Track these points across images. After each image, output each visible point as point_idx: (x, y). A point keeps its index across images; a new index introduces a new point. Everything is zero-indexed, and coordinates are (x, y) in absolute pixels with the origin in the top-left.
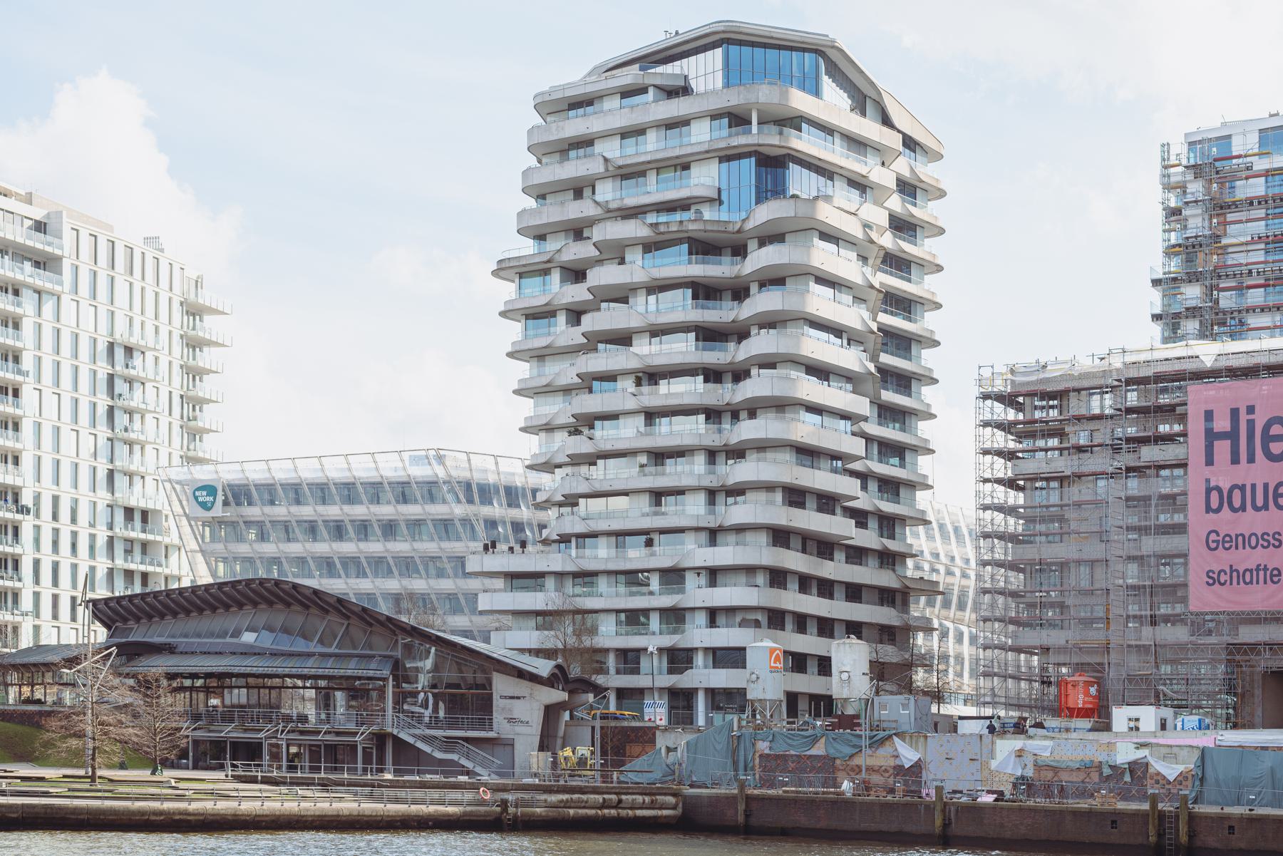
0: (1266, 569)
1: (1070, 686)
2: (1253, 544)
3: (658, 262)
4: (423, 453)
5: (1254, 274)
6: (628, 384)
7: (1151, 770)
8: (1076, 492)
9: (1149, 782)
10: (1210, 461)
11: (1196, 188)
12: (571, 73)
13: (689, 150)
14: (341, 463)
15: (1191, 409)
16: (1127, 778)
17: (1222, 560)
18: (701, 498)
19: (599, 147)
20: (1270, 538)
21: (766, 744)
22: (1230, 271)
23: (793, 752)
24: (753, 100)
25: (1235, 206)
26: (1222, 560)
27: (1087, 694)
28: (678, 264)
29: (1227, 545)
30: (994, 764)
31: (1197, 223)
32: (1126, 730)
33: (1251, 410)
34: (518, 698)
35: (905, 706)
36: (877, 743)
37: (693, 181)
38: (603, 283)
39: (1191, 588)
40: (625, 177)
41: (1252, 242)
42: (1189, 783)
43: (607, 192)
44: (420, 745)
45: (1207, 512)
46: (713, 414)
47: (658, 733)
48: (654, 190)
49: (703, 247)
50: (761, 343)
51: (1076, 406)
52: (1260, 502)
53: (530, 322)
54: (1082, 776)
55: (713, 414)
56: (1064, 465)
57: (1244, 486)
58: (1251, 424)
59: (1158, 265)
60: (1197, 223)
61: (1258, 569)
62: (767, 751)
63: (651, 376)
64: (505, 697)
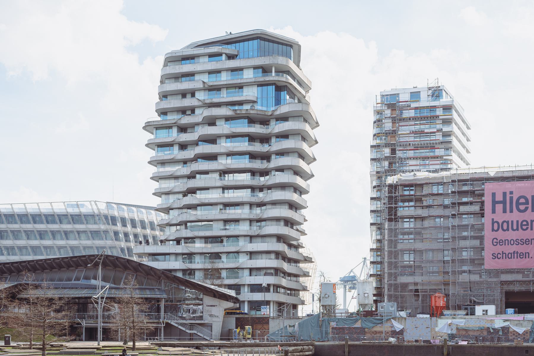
0: (517, 253)
1: (437, 298)
2: (512, 243)
3: (232, 126)
4: (75, 203)
5: (411, 145)
6: (216, 176)
7: (511, 330)
8: (426, 223)
9: (510, 334)
10: (494, 211)
11: (388, 112)
12: (180, 45)
13: (242, 81)
14: (10, 207)
15: (486, 192)
16: (501, 333)
17: (499, 249)
18: (248, 223)
19: (197, 77)
20: (519, 241)
21: (335, 323)
22: (402, 144)
23: (346, 326)
24: (276, 63)
25: (404, 120)
26: (499, 249)
27: (444, 301)
28: (243, 127)
29: (501, 244)
30: (437, 329)
31: (388, 125)
32: (482, 314)
33: (511, 193)
34: (214, 306)
35: (392, 307)
36: (381, 322)
37: (244, 94)
38: (209, 133)
39: (485, 260)
40: (210, 90)
41: (410, 133)
42: (528, 334)
43: (201, 96)
44: (180, 327)
45: (493, 231)
46: (253, 189)
47: (270, 320)
48: (224, 96)
49: (252, 121)
50: (277, 162)
51: (426, 190)
52: (515, 228)
53: (160, 149)
54: (479, 333)
55: (253, 189)
56: (420, 212)
57: (508, 221)
58: (511, 199)
59: (371, 141)
60: (388, 125)
61: (514, 253)
62: (335, 326)
63: (223, 173)
64: (209, 306)
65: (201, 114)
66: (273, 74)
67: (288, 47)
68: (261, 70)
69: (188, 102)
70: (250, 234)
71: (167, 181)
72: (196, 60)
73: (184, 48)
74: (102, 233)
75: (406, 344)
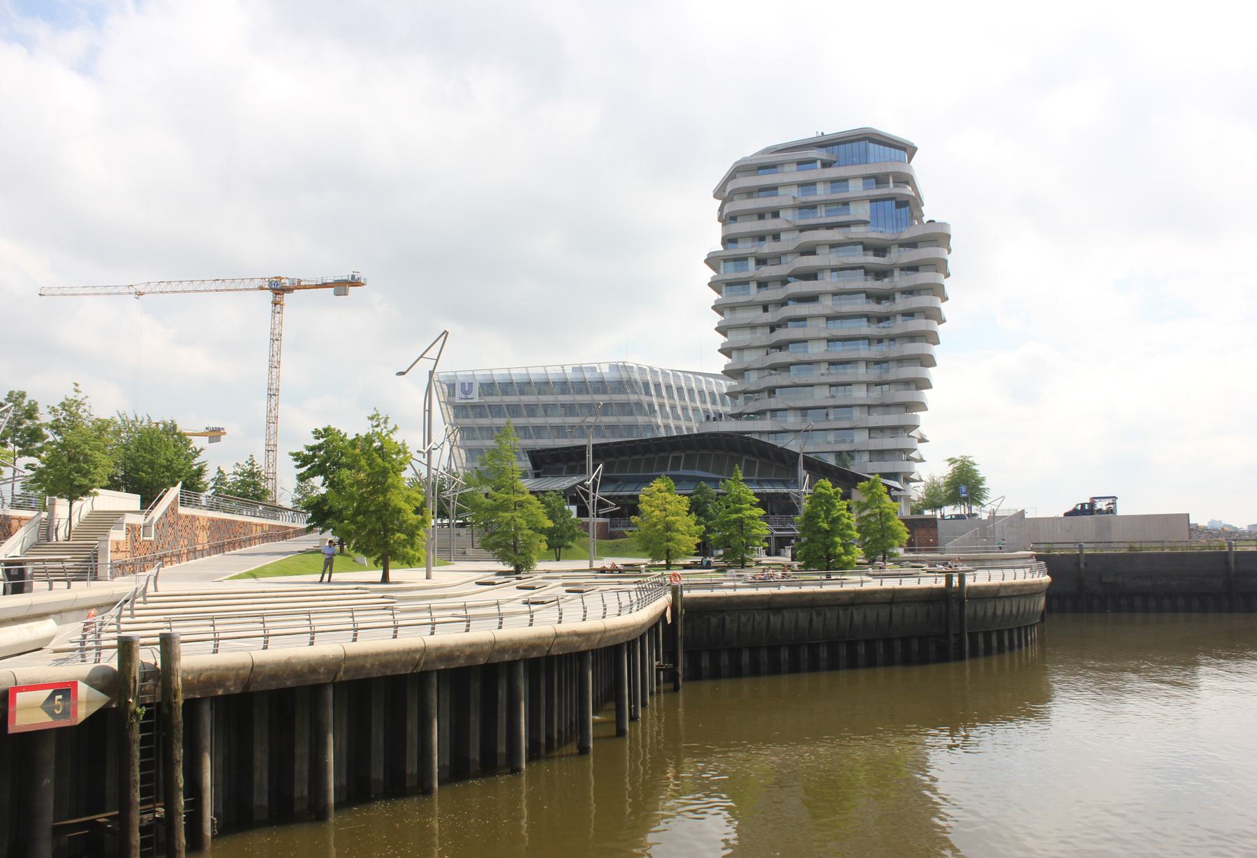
65: (789, 241)
66: (891, 185)
67: (908, 150)
68: (873, 180)
69: (769, 224)
70: (869, 403)
71: (739, 332)
72: (779, 169)
73: (757, 154)
74: (577, 408)
75: (447, 763)
